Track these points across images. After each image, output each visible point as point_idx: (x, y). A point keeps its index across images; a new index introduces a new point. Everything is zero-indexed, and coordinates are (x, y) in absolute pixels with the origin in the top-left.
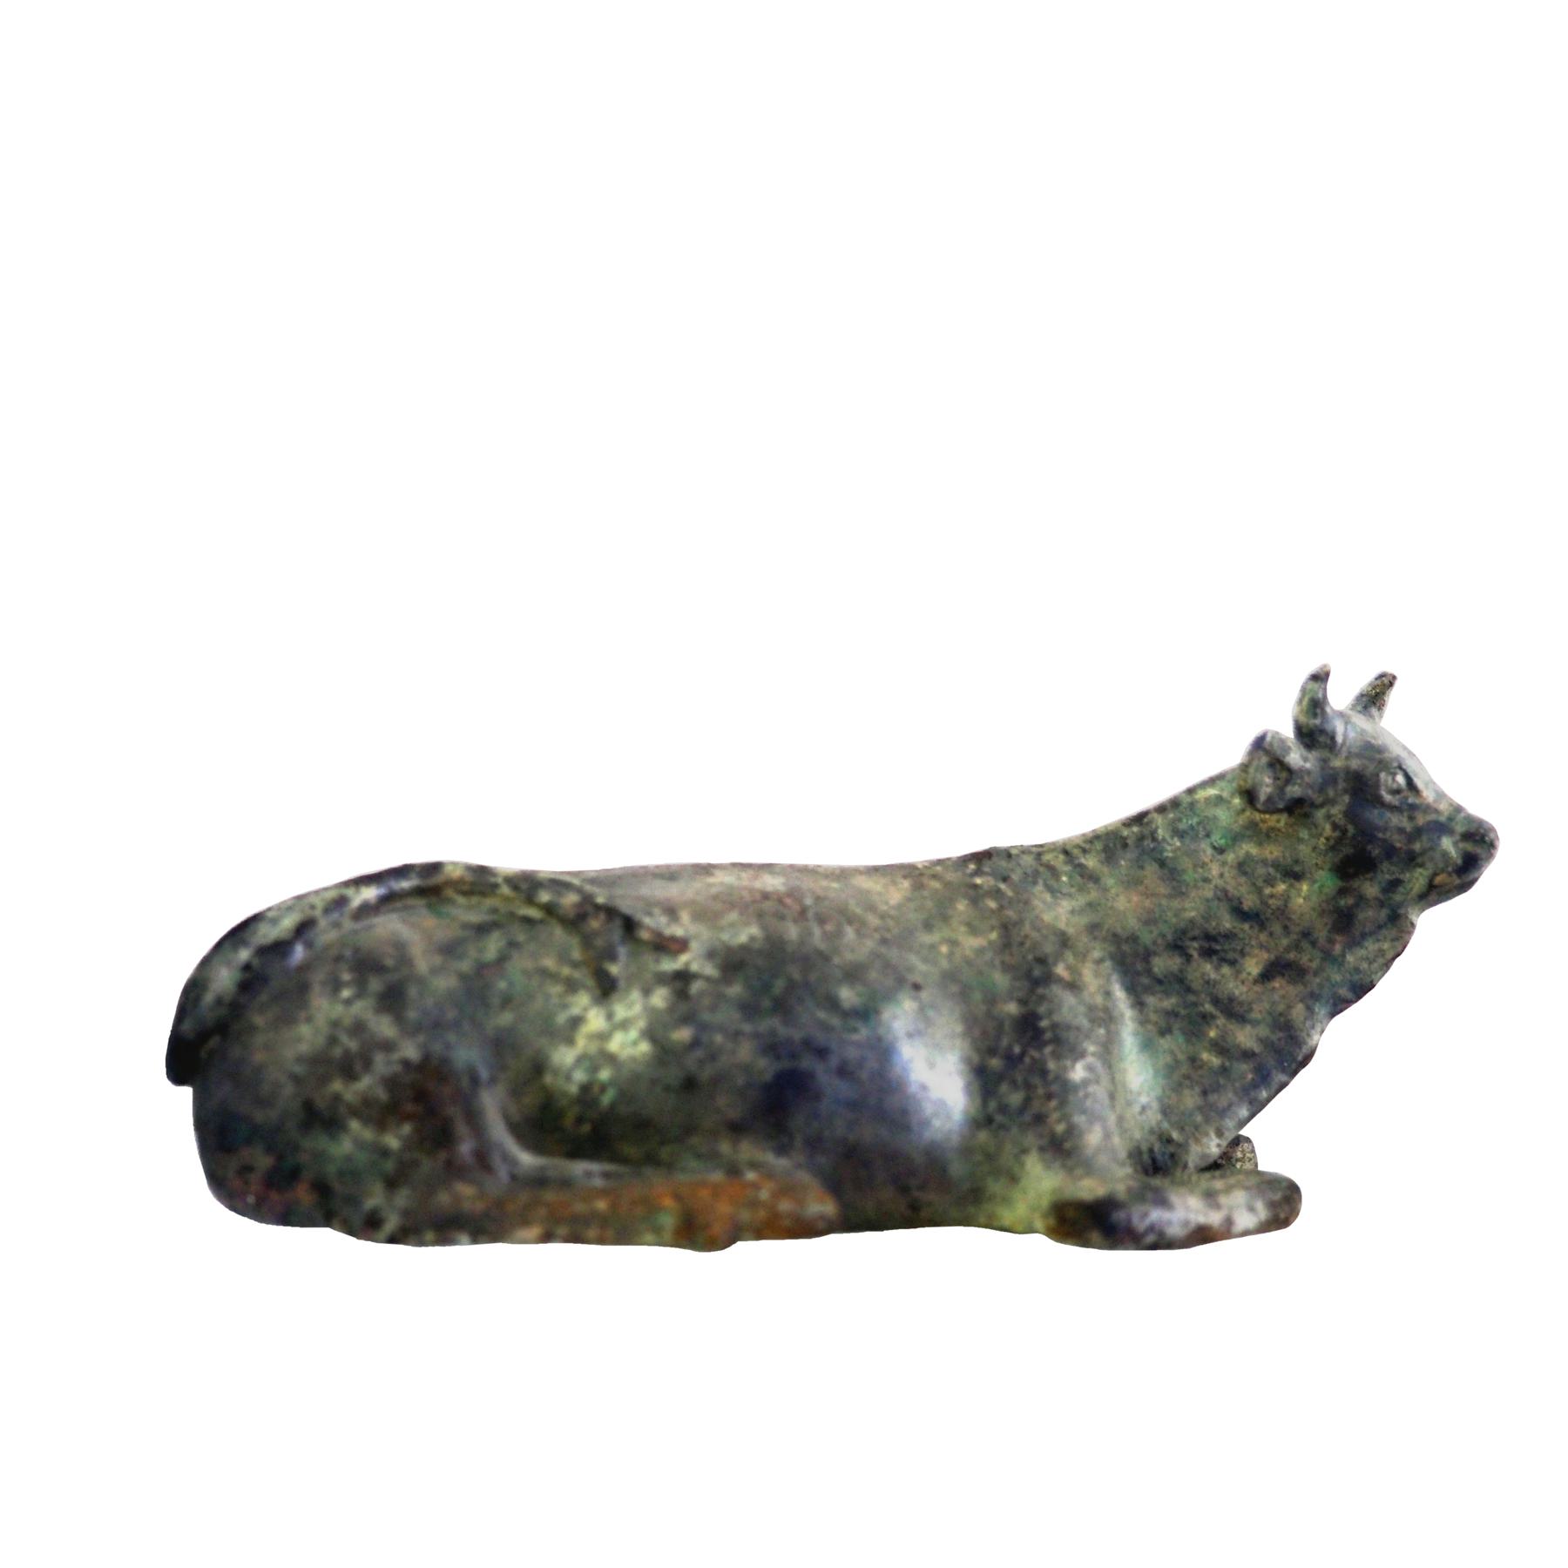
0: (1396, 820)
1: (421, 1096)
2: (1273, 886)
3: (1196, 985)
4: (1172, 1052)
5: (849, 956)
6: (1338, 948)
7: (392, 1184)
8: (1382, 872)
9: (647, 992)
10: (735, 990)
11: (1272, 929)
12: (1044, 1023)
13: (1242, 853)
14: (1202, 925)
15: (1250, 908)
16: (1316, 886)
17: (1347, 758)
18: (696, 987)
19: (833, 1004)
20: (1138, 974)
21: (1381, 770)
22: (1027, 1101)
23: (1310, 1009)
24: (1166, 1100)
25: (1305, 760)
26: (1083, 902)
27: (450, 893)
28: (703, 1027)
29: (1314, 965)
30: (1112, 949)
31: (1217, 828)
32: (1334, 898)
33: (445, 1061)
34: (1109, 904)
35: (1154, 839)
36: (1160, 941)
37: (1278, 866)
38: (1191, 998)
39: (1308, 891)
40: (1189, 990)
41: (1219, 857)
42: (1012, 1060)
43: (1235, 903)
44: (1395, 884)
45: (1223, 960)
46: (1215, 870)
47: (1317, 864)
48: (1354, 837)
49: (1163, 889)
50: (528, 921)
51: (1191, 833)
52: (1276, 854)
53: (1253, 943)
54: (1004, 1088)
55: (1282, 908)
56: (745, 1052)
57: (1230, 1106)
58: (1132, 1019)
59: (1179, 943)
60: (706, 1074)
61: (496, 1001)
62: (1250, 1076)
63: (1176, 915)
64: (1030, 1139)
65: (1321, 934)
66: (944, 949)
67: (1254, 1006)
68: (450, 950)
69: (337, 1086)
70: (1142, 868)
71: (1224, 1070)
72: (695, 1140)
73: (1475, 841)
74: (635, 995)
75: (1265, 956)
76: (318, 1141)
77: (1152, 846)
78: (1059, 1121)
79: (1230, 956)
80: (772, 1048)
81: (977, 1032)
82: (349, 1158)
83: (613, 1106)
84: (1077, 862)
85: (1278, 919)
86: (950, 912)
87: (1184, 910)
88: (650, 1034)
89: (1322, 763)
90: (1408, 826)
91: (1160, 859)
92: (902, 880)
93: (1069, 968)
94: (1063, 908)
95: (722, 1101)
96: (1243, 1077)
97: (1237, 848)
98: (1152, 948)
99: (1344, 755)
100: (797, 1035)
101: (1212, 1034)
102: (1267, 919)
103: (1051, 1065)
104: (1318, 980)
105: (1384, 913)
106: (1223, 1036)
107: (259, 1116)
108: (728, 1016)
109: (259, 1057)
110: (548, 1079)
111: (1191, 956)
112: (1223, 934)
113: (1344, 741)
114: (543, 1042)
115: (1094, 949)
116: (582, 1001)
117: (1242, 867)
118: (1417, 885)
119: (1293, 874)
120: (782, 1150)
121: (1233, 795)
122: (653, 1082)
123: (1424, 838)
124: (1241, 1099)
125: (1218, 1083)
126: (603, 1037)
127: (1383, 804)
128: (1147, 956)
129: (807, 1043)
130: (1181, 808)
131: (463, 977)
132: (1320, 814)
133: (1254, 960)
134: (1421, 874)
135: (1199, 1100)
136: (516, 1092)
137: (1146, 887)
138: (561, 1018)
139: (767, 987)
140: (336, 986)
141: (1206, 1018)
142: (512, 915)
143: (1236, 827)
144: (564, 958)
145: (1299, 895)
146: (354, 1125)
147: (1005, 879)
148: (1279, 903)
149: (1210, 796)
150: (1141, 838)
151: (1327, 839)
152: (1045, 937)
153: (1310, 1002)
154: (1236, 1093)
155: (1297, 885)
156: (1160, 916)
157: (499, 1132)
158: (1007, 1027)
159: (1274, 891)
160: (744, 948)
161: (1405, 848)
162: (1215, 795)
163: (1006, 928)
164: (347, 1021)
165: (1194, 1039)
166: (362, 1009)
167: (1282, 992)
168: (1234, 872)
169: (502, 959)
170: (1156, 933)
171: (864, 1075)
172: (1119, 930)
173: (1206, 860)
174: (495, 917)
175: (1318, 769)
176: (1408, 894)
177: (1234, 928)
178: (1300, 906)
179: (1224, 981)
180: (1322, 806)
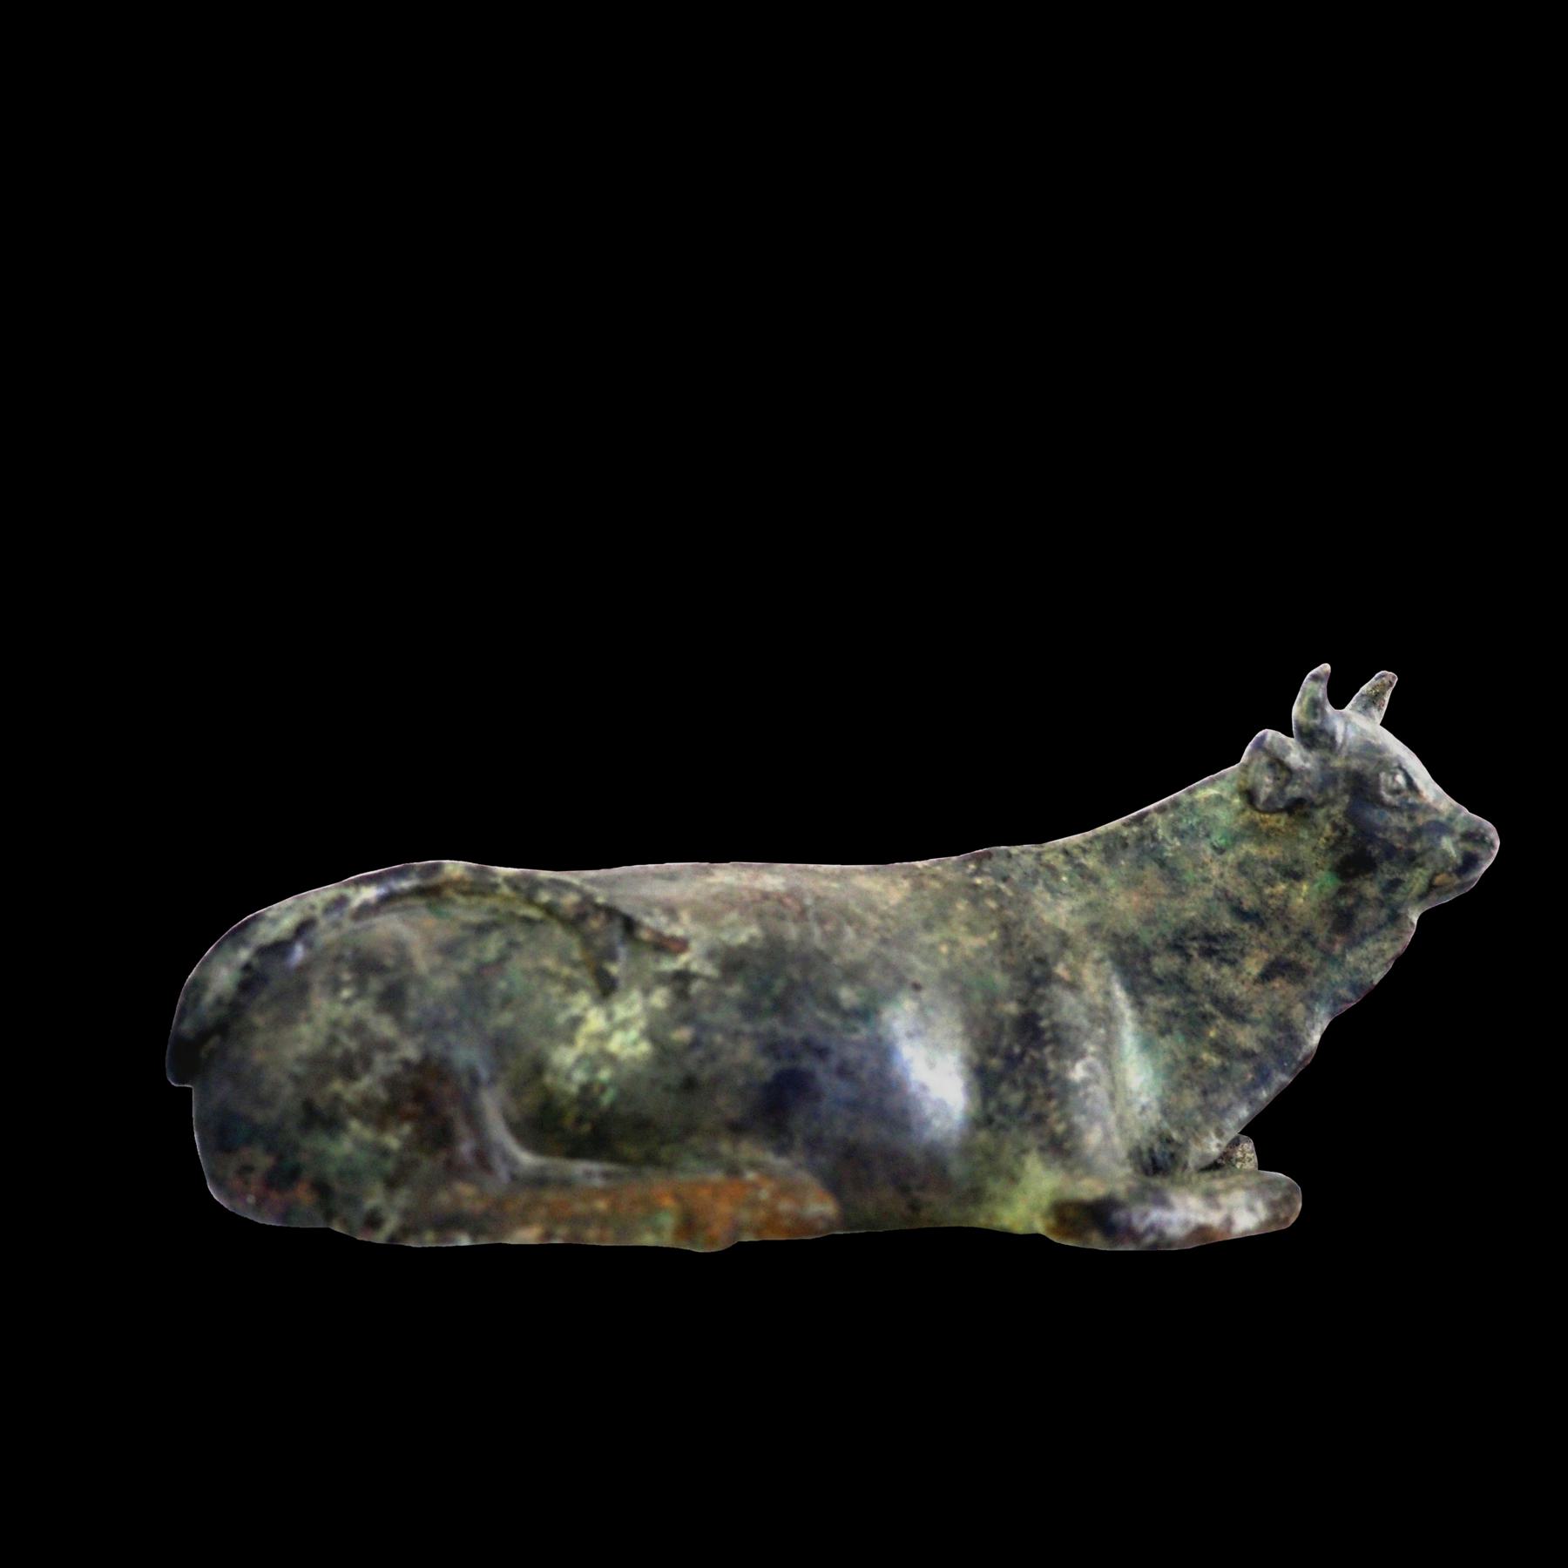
0: (1396, 820)
1: (421, 1096)
2: (1273, 886)
3: (1196, 985)
4: (1172, 1052)
5: (849, 956)
6: (1338, 948)
7: (392, 1184)
8: (1382, 872)
9: (647, 992)
10: (735, 990)
11: (1272, 929)
12: (1044, 1023)
13: (1242, 853)
14: (1202, 925)
15: (1250, 908)
16: (1316, 886)
17: (1347, 758)
18: (696, 987)
19: (833, 1004)
20: (1138, 974)
21: (1381, 770)
22: (1027, 1101)
23: (1310, 1009)
24: (1166, 1100)
25: (1305, 760)
26: (1083, 902)
27: (450, 893)
28: (703, 1027)
29: (1314, 965)
30: (1112, 949)
31: (1217, 828)
32: (1334, 898)
33: (445, 1061)
34: (1109, 904)
35: (1154, 839)
36: (1160, 941)
37: (1278, 866)
38: (1191, 998)
39: (1308, 891)
40: (1189, 990)
41: (1219, 857)
42: (1012, 1060)
43: (1235, 903)
44: (1395, 884)
45: (1223, 960)
46: (1215, 870)
47: (1317, 864)
48: (1354, 837)
49: (1163, 889)
50: (528, 921)
51: (1191, 833)
52: (1276, 854)
53: (1253, 943)
54: (1004, 1088)
55: (1282, 908)
56: (745, 1052)
57: (1230, 1106)
58: (1132, 1019)
59: (1179, 943)
60: (706, 1074)
61: (496, 1001)
62: (1250, 1076)
63: (1176, 915)
64: (1030, 1139)
65: (1321, 934)
66: (944, 949)
67: (1254, 1006)
68: (450, 950)
69: (337, 1086)
70: (1142, 868)
71: (1224, 1070)
72: (695, 1140)
74: (635, 995)
75: (1265, 956)
76: (318, 1141)
77: (1152, 846)
78: (1059, 1121)
79: (1230, 956)
80: (772, 1048)
81: (977, 1032)
82: (349, 1158)
83: (613, 1106)
84: (1077, 862)
85: (1278, 919)
86: (950, 912)
87: (1184, 910)
88: (650, 1034)
89: (1322, 763)
90: (1408, 826)
91: (1160, 859)
92: (902, 880)
93: (1069, 968)
94: (1063, 908)
95: (722, 1101)
96: (1243, 1077)
97: (1237, 848)
98: (1152, 948)
99: (1344, 755)
100: (797, 1035)
101: (1212, 1034)
102: (1267, 919)
103: (1051, 1065)
104: (1318, 980)
105: (1384, 913)
106: (1223, 1036)
107: (259, 1116)
108: (728, 1016)
109: (259, 1057)
110: (548, 1079)
111: (1191, 956)
112: (1223, 934)
113: (1344, 741)
114: (543, 1042)
115: (1094, 949)
116: (582, 1001)
117: (1242, 867)
118: (1417, 885)
119: (1293, 874)
120: (782, 1150)
121: (1233, 795)
122: (653, 1082)
123: (1424, 838)
124: (1241, 1099)
125: (1218, 1083)
126: (603, 1037)
127: (1383, 804)
128: (1147, 956)
129: (807, 1043)
130: (1181, 808)
131: (463, 977)
132: (1320, 814)
133: (1254, 960)
134: (1421, 874)
135: (1199, 1100)
136: (516, 1092)
137: (1146, 887)
138: (561, 1018)
139: (767, 987)
140: (336, 986)
141: (1206, 1018)
142: (512, 915)
143: (1236, 827)
144: (564, 958)
145: (1299, 895)
146: (354, 1125)
147: (1005, 879)
148: (1279, 903)
149: (1210, 796)
150: (1141, 838)
151: (1327, 839)
152: (1045, 937)
153: (1310, 1002)
154: (1236, 1093)
155: (1297, 885)
156: (1160, 916)
157: (499, 1132)
158: (1007, 1027)
159: (1274, 891)
160: (744, 948)
161: (1405, 848)
162: (1215, 795)
163: (1006, 928)
164: (347, 1021)
165: (1194, 1039)
166: (362, 1009)
167: (1282, 992)
168: (1234, 872)
169: (502, 959)
170: (1156, 933)
171: (864, 1075)
172: (1119, 930)
173: (1206, 860)
174: (495, 917)
175: (1318, 769)
176: (1408, 894)
177: (1234, 928)
179: (1224, 981)
180: (1322, 806)
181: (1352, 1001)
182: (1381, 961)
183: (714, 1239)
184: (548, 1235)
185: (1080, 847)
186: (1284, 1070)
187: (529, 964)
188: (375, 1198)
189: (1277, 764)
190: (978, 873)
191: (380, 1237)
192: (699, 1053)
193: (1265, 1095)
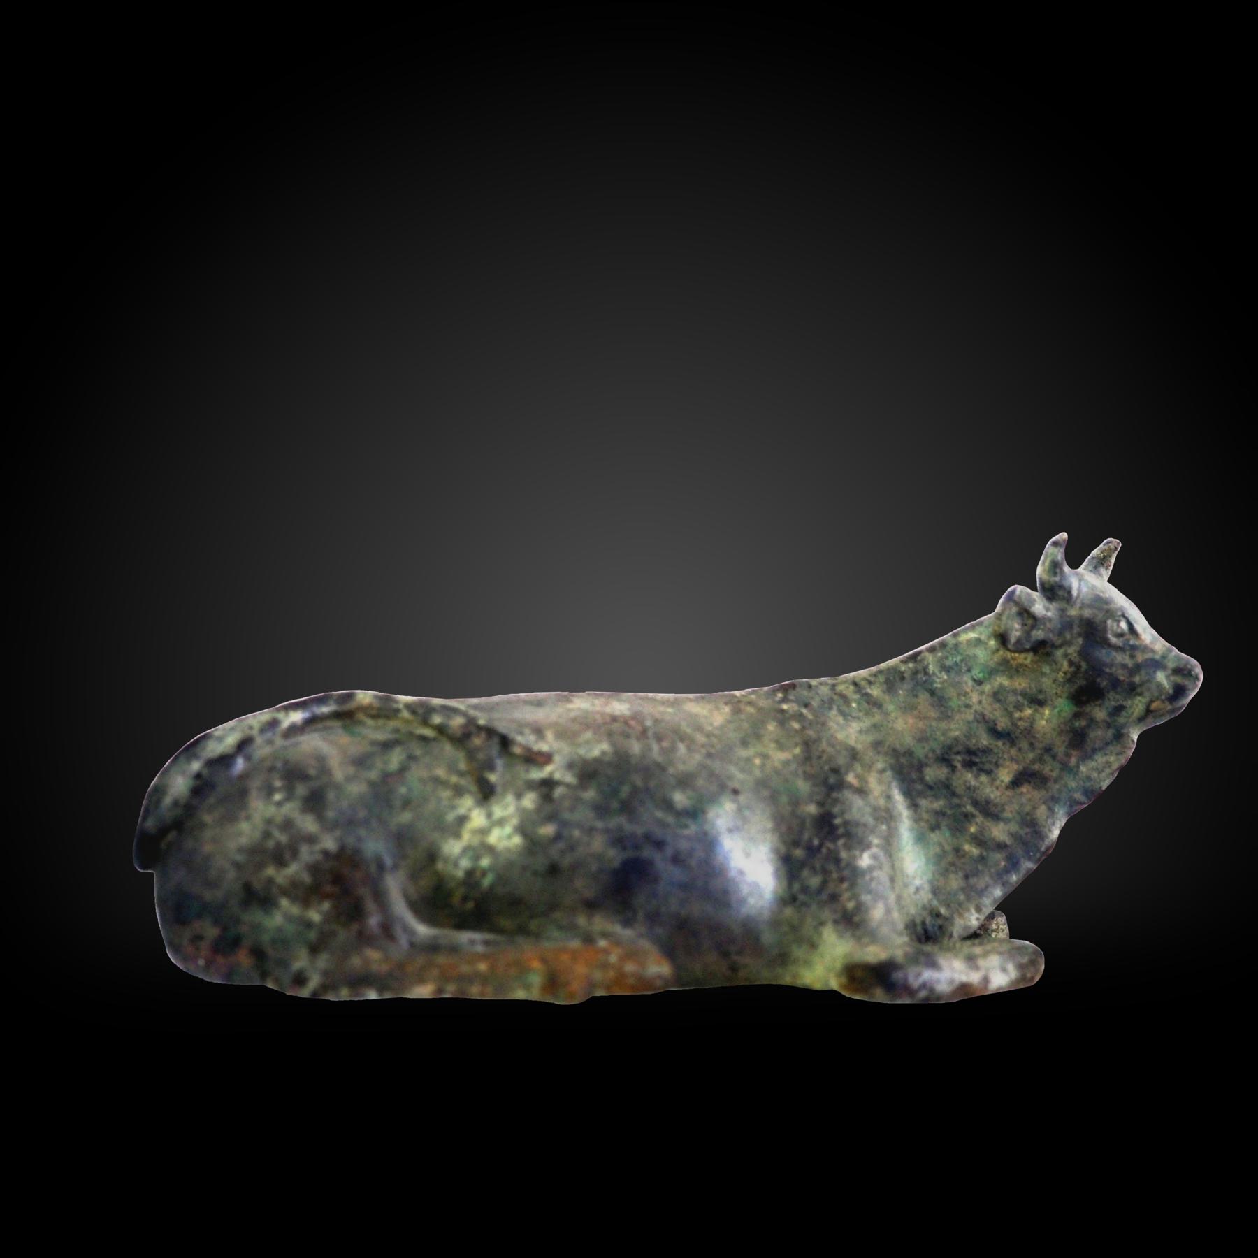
0: (1120, 658)
1: (338, 879)
2: (1021, 711)
3: (960, 791)
4: (940, 844)
5: (681, 767)
6: (1073, 761)
7: (314, 950)
8: (1109, 699)
9: (519, 796)
10: (590, 794)
11: (1020, 745)
12: (838, 821)
13: (996, 684)
14: (964, 742)
15: (1003, 728)
16: (1056, 710)
17: (1081, 608)
18: (558, 792)
19: (668, 805)
20: (913, 781)
21: (1108, 618)
22: (824, 884)
23: (1051, 810)
24: (936, 883)
25: (1047, 609)
26: (869, 723)
27: (361, 716)
28: (564, 824)
29: (1054, 774)
30: (893, 761)
31: (976, 664)
32: (1070, 720)
33: (357, 851)
34: (890, 725)
35: (926, 673)
36: (930, 755)
37: (1026, 695)
38: (956, 801)
39: (1049, 714)
40: (954, 794)
41: (978, 688)
42: (812, 851)
43: (991, 725)
44: (1119, 709)
45: (981, 770)
46: (975, 698)
47: (1056, 693)
48: (1086, 672)
49: (933, 714)
50: (424, 739)
51: (955, 668)
52: (1023, 685)
53: (1006, 756)
54: (805, 873)
55: (1029, 728)
56: (598, 844)
57: (987, 887)
58: (908, 817)
59: (946, 757)
60: (566, 862)
61: (398, 803)
62: (1003, 864)
63: (943, 734)
64: (827, 914)
65: (1060, 749)
66: (757, 761)
67: (1006, 807)
68: (361, 762)
69: (270, 871)
70: (916, 696)
71: (982, 859)
72: (557, 915)
73: (1184, 675)
74: (510, 798)
75: (1015, 767)
76: (255, 916)
77: (924, 679)
78: (850, 899)
79: (987, 767)
80: (619, 840)
81: (784, 828)
82: (280, 929)
83: (492, 887)
84: (864, 691)
85: (1025, 737)
86: (762, 732)
87: (950, 730)
88: (522, 830)
89: (1060, 612)
90: (1130, 663)
91: (930, 690)
92: (724, 706)
93: (858, 777)
94: (853, 728)
95: (579, 883)
96: (997, 864)
97: (992, 681)
98: (925, 760)
99: (1078, 605)
100: (639, 830)
101: (973, 829)
102: (1017, 737)
103: (843, 855)
104: (1057, 786)
105: (1110, 733)
106: (982, 831)
107: (208, 896)
108: (584, 815)
109: (208, 848)
110: (440, 866)
111: (956, 767)
113: (1079, 594)
114: (435, 836)
115: (878, 761)
116: (467, 803)
117: (997, 696)
118: (1137, 710)
119: (1038, 702)
120: (627, 923)
121: (989, 638)
122: (524, 868)
123: (1143, 672)
124: (995, 882)
125: (977, 869)
126: (484, 832)
127: (1109, 645)
128: (920, 767)
129: (648, 837)
130: (948, 648)
131: (371, 784)
132: (1059, 653)
133: (1006, 771)
134: (1140, 701)
135: (962, 883)
136: (414, 876)
137: (920, 712)
138: (450, 817)
139: (615, 792)
140: (269, 791)
141: (968, 817)
142: (411, 734)
143: (992, 664)
144: (452, 768)
145: (1043, 718)
146: (284, 902)
147: (806, 705)
148: (1026, 724)
149: (971, 639)
150: (915, 672)
151: (1065, 673)
152: (839, 752)
153: (1051, 804)
154: (991, 877)
155: (1041, 710)
156: (931, 735)
157: (400, 908)
158: (808, 824)
159: (1022, 715)
160: (597, 761)
161: (1127, 680)
162: (975, 638)
163: (807, 744)
164: (279, 819)
165: (958, 834)
166: (291, 809)
167: (1028, 796)
168: (990, 699)
169: (403, 770)
170: (927, 748)
171: (693, 863)
172: (898, 747)
173: (968, 690)
174: (397, 736)
175: (1057, 617)
176: (1130, 717)
177: (990, 744)
178: (1043, 727)
179: (982, 787)
180: (1060, 646)
181: (1084, 803)
182: (1108, 771)
183: (573, 994)
184: (440, 990)
185: (867, 680)
186: (1030, 859)
187: (424, 774)
188: (301, 961)
189: (1025, 613)
190: (784, 700)
191: (305, 993)
192: (561, 845)
193: (1014, 878)
